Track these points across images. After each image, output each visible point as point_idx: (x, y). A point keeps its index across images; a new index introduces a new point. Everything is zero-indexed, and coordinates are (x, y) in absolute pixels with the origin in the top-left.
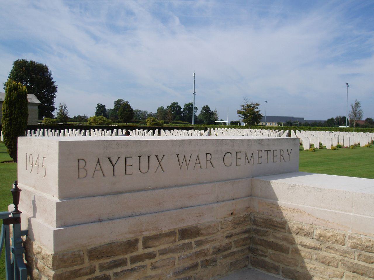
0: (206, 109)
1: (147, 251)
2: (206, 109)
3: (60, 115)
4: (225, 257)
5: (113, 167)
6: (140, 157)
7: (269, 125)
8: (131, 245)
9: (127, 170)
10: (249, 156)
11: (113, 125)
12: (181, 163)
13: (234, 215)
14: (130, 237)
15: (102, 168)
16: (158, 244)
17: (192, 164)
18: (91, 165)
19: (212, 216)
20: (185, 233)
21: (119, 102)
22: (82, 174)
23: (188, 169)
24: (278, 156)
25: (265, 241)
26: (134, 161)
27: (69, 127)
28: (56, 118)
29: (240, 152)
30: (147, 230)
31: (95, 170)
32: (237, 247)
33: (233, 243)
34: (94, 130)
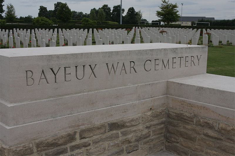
0: (131, 10)
1: (83, 140)
2: (131, 10)
3: (8, 15)
4: (145, 143)
5: (55, 76)
6: (76, 67)
7: (184, 24)
8: (71, 137)
9: (67, 77)
10: (165, 63)
11: (54, 25)
12: (110, 70)
13: (152, 110)
14: (70, 131)
15: (46, 77)
16: (92, 134)
17: (118, 71)
18: (37, 75)
19: (135, 112)
20: (114, 126)
21: (58, 5)
22: (30, 81)
23: (116, 75)
24: (190, 62)
25: (177, 130)
26: (72, 70)
27: (16, 27)
28: (4, 19)
29: (158, 59)
30: (83, 125)
31: (41, 79)
32: (155, 135)
33: (151, 132)
34: (38, 29)
